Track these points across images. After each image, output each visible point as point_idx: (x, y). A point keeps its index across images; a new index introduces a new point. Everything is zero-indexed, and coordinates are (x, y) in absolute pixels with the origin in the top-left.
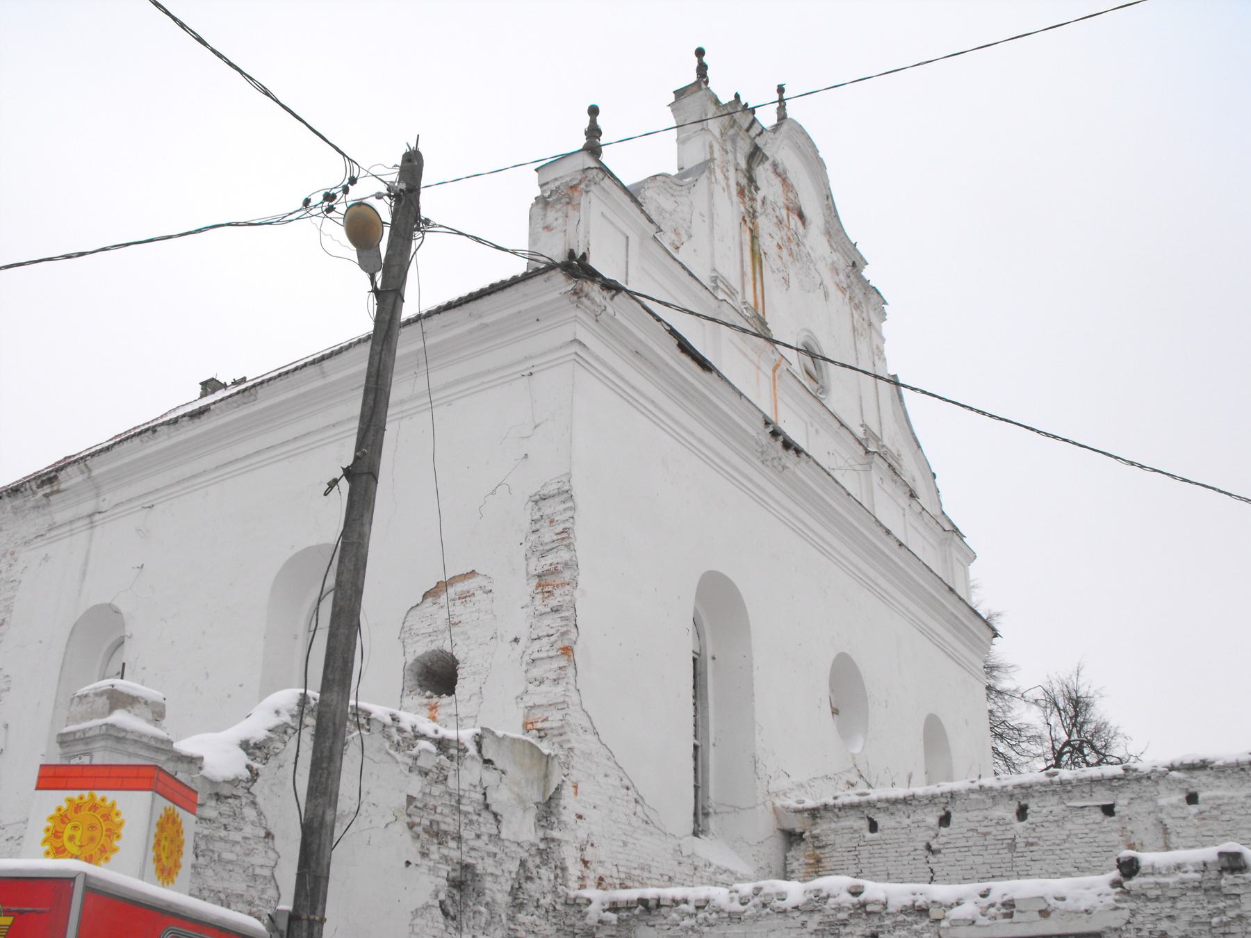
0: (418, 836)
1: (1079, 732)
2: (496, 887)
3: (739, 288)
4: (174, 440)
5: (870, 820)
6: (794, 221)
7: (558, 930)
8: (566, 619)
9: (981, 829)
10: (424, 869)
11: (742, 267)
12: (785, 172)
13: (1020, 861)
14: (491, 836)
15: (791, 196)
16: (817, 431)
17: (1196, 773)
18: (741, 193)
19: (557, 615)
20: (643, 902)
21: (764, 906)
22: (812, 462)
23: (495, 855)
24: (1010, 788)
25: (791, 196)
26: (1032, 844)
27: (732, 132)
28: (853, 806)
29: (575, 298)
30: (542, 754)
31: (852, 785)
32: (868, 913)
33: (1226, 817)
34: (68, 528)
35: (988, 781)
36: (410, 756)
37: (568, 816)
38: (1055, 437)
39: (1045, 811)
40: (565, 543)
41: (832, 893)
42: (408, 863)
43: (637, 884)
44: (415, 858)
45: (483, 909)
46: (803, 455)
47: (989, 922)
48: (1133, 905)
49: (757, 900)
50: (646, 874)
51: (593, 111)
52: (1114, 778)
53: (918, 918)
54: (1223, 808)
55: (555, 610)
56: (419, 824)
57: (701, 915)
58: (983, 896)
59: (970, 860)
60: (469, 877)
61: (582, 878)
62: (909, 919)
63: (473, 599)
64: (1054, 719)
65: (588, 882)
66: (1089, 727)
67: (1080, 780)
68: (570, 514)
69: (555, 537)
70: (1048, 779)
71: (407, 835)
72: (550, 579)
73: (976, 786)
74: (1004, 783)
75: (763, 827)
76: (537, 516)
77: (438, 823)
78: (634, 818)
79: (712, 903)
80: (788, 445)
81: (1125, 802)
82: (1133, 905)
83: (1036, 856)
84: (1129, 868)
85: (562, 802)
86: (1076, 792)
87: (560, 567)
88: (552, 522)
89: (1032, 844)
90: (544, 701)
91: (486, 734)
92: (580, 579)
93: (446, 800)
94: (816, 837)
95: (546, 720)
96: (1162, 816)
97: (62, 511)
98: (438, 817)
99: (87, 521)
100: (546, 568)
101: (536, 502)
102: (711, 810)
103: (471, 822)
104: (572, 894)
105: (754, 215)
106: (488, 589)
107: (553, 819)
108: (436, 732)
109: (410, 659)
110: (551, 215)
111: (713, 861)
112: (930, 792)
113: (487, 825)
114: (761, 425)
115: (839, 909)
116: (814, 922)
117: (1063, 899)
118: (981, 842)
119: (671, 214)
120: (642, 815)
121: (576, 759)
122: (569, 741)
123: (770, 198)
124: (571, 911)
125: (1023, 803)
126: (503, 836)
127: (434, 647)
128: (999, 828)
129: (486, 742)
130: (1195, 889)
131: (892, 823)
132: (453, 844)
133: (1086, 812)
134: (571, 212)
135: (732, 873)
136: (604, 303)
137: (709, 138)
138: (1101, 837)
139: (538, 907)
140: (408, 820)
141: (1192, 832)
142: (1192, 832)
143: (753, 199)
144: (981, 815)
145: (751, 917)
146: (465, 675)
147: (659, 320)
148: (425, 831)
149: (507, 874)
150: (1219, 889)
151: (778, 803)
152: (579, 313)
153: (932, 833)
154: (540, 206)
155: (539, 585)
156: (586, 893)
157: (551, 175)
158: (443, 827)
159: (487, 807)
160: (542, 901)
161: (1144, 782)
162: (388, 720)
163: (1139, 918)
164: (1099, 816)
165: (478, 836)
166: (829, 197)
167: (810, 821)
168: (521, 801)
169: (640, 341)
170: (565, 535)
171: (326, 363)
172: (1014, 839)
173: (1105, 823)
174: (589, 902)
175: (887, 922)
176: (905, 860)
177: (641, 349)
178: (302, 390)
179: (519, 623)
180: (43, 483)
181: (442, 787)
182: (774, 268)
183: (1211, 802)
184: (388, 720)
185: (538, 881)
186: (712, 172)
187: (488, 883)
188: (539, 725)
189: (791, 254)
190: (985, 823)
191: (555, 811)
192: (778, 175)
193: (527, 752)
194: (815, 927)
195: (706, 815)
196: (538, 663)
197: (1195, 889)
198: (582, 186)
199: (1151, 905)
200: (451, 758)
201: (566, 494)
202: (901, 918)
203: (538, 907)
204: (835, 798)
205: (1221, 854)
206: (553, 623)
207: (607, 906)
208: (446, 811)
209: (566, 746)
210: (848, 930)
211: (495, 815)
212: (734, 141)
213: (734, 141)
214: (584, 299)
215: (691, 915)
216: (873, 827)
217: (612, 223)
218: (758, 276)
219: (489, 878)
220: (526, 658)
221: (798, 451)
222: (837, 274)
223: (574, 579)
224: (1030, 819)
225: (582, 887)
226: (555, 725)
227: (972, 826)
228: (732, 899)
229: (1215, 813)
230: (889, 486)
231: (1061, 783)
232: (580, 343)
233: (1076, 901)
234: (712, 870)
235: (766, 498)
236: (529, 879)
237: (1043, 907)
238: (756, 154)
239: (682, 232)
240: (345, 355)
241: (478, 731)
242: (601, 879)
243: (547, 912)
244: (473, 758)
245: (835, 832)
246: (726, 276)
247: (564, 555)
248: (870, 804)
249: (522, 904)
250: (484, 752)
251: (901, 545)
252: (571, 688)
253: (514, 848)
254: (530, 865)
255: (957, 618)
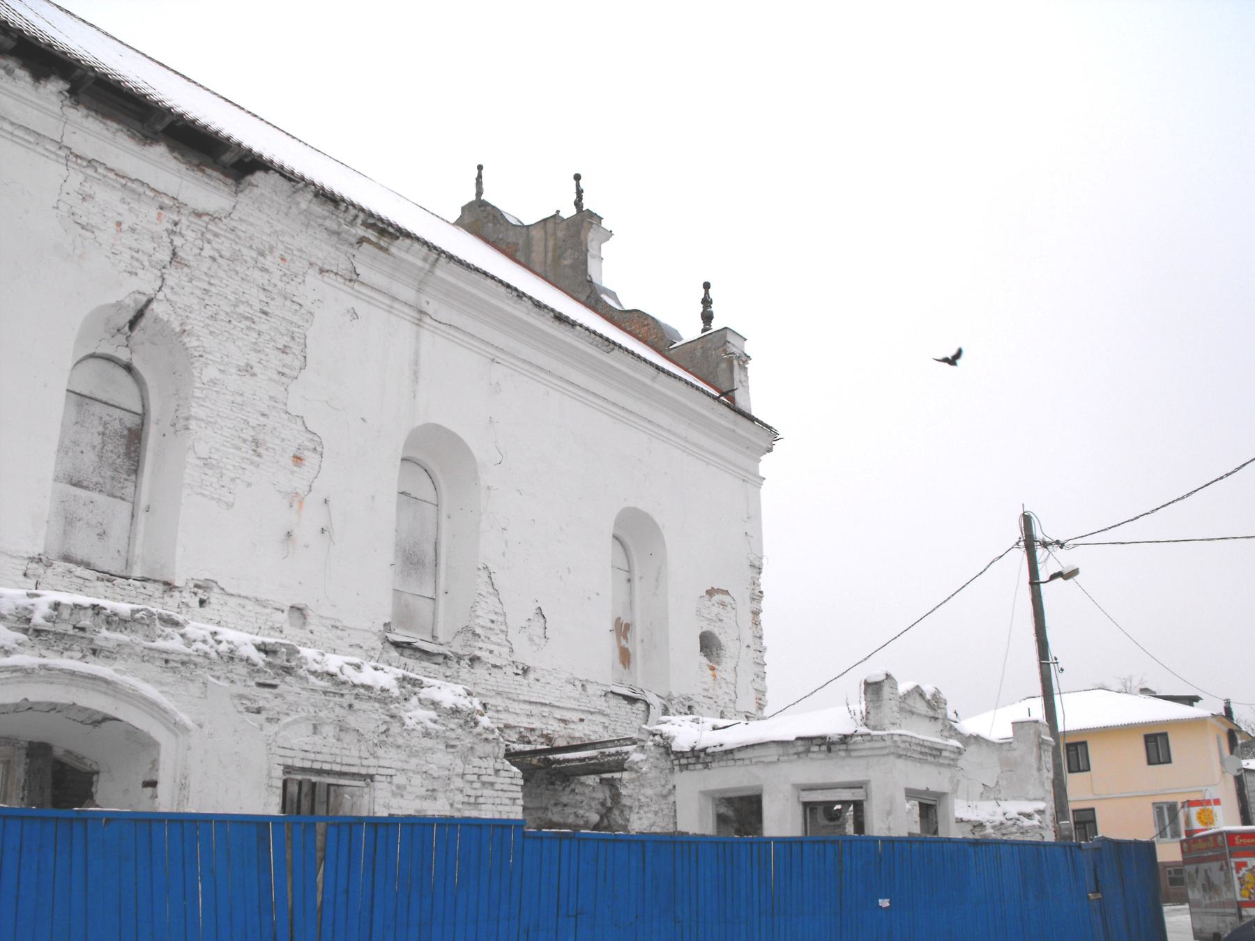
4: (530, 320)
34: (387, 301)
97: (369, 265)
99: (416, 315)
171: (662, 375)
178: (461, 285)
180: (372, 226)
240: (643, 364)
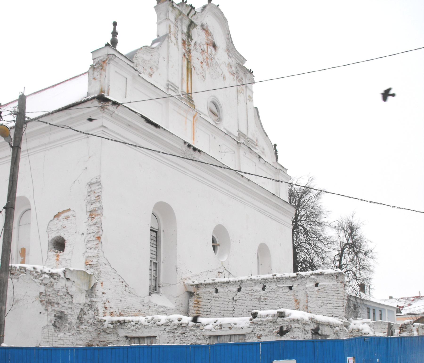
0: (44, 304)
1: (352, 239)
2: (72, 318)
3: (180, 86)
5: (216, 289)
6: (211, 48)
7: (95, 330)
8: (98, 227)
9: (250, 293)
10: (46, 314)
11: (182, 76)
12: (207, 27)
13: (262, 305)
14: (70, 302)
15: (210, 38)
16: (215, 138)
17: (319, 276)
18: (184, 43)
19: (96, 226)
20: (119, 322)
21: (154, 323)
22: (206, 155)
23: (71, 308)
24: (260, 280)
25: (210, 38)
26: (266, 299)
27: (180, 17)
28: (210, 284)
29: (102, 109)
30: (88, 274)
31: (221, 273)
32: (183, 327)
33: (325, 291)
35: (253, 277)
36: (40, 280)
37: (99, 293)
38: (248, 173)
39: (271, 288)
40: (98, 200)
41: (173, 320)
42: (41, 313)
43: (126, 314)
44: (43, 311)
45: (67, 325)
46: (202, 153)
47: (215, 330)
48: (254, 326)
49: (152, 322)
50: (129, 310)
51: (115, 24)
52: (293, 277)
53: (197, 329)
54: (325, 288)
55: (95, 224)
56: (44, 301)
57: (137, 326)
58: (215, 322)
59: (246, 304)
60: (63, 315)
61: (104, 313)
62: (194, 329)
63: (70, 219)
64: (342, 234)
65: (107, 314)
66: (356, 237)
67: (283, 278)
68: (100, 190)
69: (95, 198)
70: (272, 277)
71: (40, 304)
72: (94, 213)
73: (249, 278)
74: (259, 278)
75: (179, 290)
76: (89, 191)
77: (51, 299)
78: (125, 292)
79: (140, 322)
80: (195, 149)
81: (296, 285)
82: (254, 326)
83: (267, 303)
84: (255, 315)
85: (96, 289)
86: (281, 282)
87: (97, 209)
88: (94, 193)
89: (266, 299)
90: (91, 255)
91: (67, 270)
92: (104, 213)
93: (53, 292)
94: (198, 294)
95: (92, 261)
96: (306, 290)
98: (50, 298)
100: (92, 209)
101: (89, 185)
102: (161, 285)
103: (63, 298)
104: (100, 318)
105: (189, 52)
106: (74, 215)
107: (93, 295)
108: (49, 271)
109: (50, 239)
110: (96, 73)
111: (157, 303)
112: (235, 280)
113: (68, 299)
114: (183, 144)
115: (174, 325)
116: (167, 329)
117: (236, 324)
118: (250, 298)
119: (149, 61)
120: (128, 291)
121: (102, 274)
122: (99, 268)
123: (199, 42)
124: (100, 324)
125: (264, 285)
126: (74, 302)
127: (57, 235)
128: (256, 293)
129: (67, 273)
130: (271, 322)
131: (222, 290)
132: (56, 306)
133: (283, 289)
134: (103, 72)
135: (166, 307)
136: (114, 110)
137: (169, 22)
138: (287, 297)
139: (88, 323)
140: (40, 299)
141: (315, 296)
142: (315, 296)
143: (189, 45)
144: (250, 288)
145: (150, 327)
146: (67, 245)
147: (136, 113)
148: (46, 302)
149: (76, 314)
150: (276, 322)
151: (186, 282)
152: (104, 115)
153: (235, 294)
154: (92, 69)
155: (90, 215)
156: (104, 318)
157: (96, 56)
158: (53, 301)
159: (68, 293)
160: (89, 321)
161: (303, 279)
162: (32, 269)
163: (255, 330)
164: (287, 290)
165: (65, 303)
166: (229, 34)
167: (196, 289)
168: (80, 290)
169: (129, 121)
170: (98, 198)
172: (260, 297)
173: (289, 293)
174: (105, 321)
175: (188, 329)
176: (226, 303)
177: (130, 124)
179: (83, 228)
181: (52, 288)
182: (198, 73)
183: (322, 286)
184: (32, 269)
185: (88, 315)
186: (169, 38)
187: (69, 317)
188: (90, 263)
189: (208, 65)
190: (252, 291)
191: (94, 292)
192: (204, 29)
193: (83, 274)
194: (168, 330)
195: (159, 287)
196: (90, 242)
197: (271, 322)
198: (107, 61)
199: (259, 326)
200: (55, 279)
201: (98, 183)
202: (192, 328)
203: (88, 323)
204: (205, 281)
205: (278, 312)
206: (94, 228)
207: (110, 322)
208: (53, 296)
209: (99, 270)
210: (177, 331)
211: (71, 295)
212: (181, 20)
213: (181, 20)
214: (105, 110)
215: (134, 326)
216: (217, 291)
217: (120, 74)
218: (189, 79)
219: (69, 315)
220: (86, 240)
221: (199, 151)
222: (231, 67)
223: (101, 213)
224: (266, 290)
225: (104, 316)
226: (95, 263)
227: (247, 292)
228: (145, 321)
229: (322, 290)
230: (248, 155)
231: (277, 278)
232: (104, 127)
233: (240, 324)
234: (157, 307)
235: (185, 170)
236: (85, 314)
237: (230, 326)
238: (191, 25)
239: (154, 68)
241: (64, 269)
242: (112, 313)
243: (91, 324)
244: (62, 278)
245: (204, 293)
246: (173, 82)
247: (98, 205)
248: (215, 284)
249: (82, 322)
250: (66, 276)
251: (249, 180)
252: (100, 251)
253: (78, 305)
254: (85, 310)
255: (277, 204)
